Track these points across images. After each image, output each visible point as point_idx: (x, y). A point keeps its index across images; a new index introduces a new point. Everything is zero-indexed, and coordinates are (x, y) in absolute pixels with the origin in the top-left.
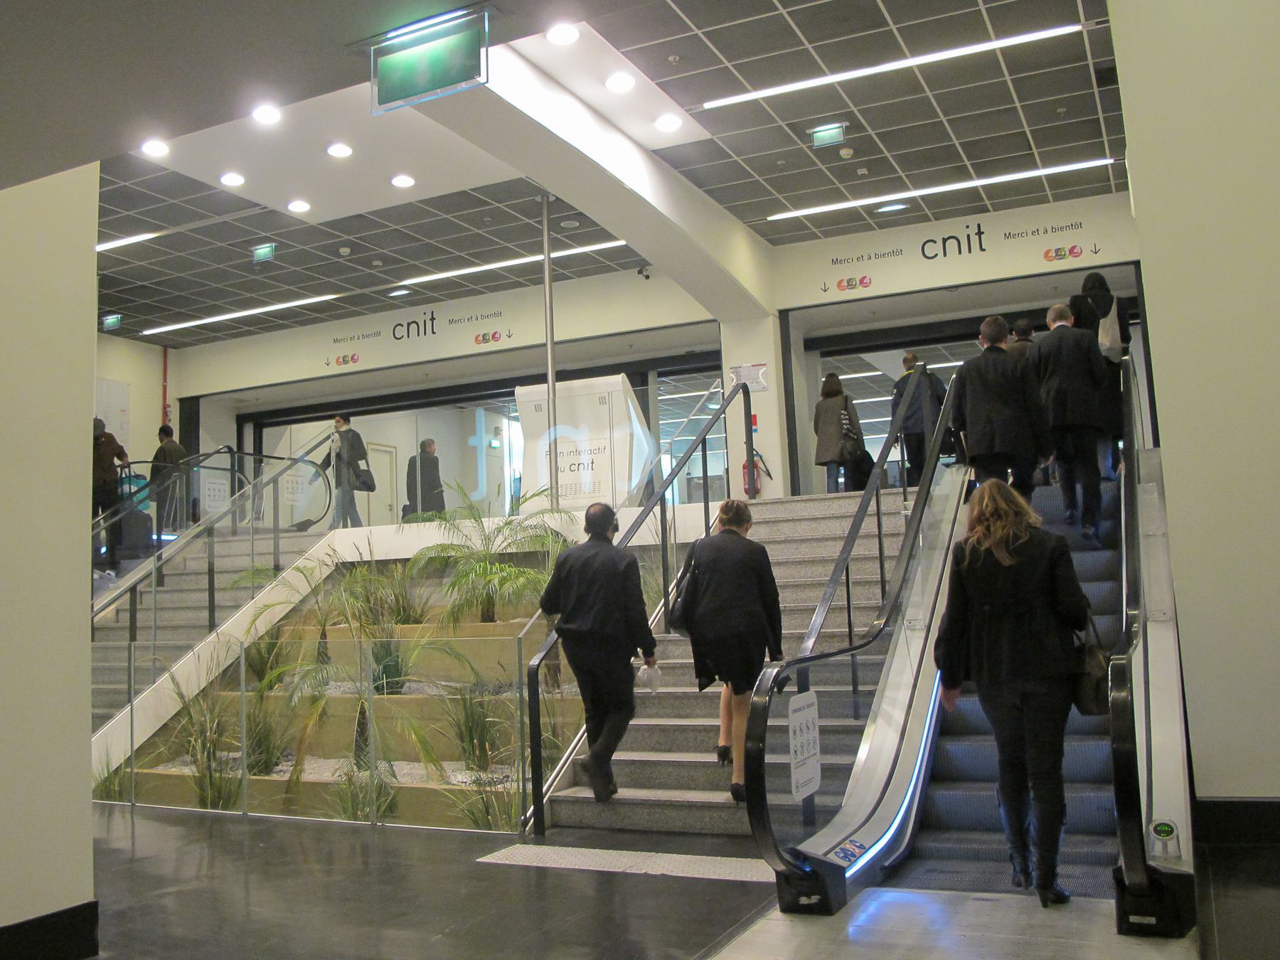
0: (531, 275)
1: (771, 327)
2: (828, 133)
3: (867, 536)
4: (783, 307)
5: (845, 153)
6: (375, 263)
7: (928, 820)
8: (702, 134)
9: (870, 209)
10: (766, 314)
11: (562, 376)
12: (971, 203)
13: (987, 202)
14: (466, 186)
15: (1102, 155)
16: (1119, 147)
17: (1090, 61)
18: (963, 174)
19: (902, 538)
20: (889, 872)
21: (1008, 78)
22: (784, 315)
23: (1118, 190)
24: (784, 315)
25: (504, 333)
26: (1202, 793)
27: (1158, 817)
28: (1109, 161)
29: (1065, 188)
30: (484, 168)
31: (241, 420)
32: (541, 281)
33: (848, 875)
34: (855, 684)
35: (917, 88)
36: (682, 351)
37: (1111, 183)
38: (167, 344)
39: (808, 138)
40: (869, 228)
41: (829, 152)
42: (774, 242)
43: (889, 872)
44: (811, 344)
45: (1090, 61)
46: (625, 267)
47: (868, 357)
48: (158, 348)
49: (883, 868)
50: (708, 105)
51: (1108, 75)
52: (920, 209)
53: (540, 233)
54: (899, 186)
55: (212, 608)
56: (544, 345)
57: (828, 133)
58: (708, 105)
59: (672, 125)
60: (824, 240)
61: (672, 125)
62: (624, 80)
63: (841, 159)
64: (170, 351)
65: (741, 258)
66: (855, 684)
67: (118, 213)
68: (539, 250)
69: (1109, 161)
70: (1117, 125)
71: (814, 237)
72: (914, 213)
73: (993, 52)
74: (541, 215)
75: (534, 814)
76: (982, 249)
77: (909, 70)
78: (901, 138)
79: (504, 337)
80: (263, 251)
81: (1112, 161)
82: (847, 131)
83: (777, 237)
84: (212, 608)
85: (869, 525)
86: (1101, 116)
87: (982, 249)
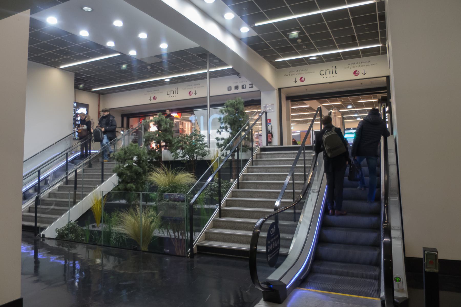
0: (203, 76)
1: (276, 93)
2: (295, 34)
3: (301, 160)
4: (279, 87)
5: (299, 41)
6: (159, 71)
7: (317, 257)
8: (255, 34)
9: (307, 58)
10: (273, 89)
11: (211, 106)
12: (337, 57)
13: (342, 57)
14: (183, 49)
15: (378, 43)
16: (384, 41)
17: (377, 13)
18: (335, 48)
19: (311, 161)
20: (302, 282)
21: (351, 18)
22: (280, 90)
23: (383, 54)
24: (280, 90)
25: (194, 93)
26: (407, 256)
27: (398, 275)
28: (380, 45)
29: (366, 53)
30: (190, 43)
31: (123, 116)
32: (206, 78)
33: (287, 287)
34: (305, 164)
35: (322, 20)
36: (250, 99)
37: (383, 51)
38: (100, 93)
39: (288, 36)
40: (306, 64)
41: (294, 40)
42: (277, 68)
43: (302, 282)
44: (288, 98)
45: (377, 13)
46: (234, 74)
47: (305, 102)
48: (97, 95)
49: (301, 280)
50: (257, 24)
51: (383, 17)
52: (322, 59)
53: (207, 62)
54: (315, 51)
55: (103, 175)
56: (207, 97)
57: (295, 34)
58: (257, 24)
59: (245, 30)
60: (292, 67)
61: (245, 30)
62: (230, 16)
63: (297, 43)
64: (101, 95)
65: (267, 72)
66: (305, 164)
67: (46, 52)
68: (205, 68)
69: (380, 45)
70: (384, 34)
71: (289, 66)
72: (320, 60)
73: (346, 9)
74: (207, 58)
75: (190, 251)
76: (336, 73)
77: (319, 15)
78: (317, 35)
79: (240, 87)
80: (124, 66)
81: (381, 45)
82: (300, 34)
83: (278, 67)
84: (103, 175)
85: (301, 158)
86: (379, 31)
87: (336, 73)
